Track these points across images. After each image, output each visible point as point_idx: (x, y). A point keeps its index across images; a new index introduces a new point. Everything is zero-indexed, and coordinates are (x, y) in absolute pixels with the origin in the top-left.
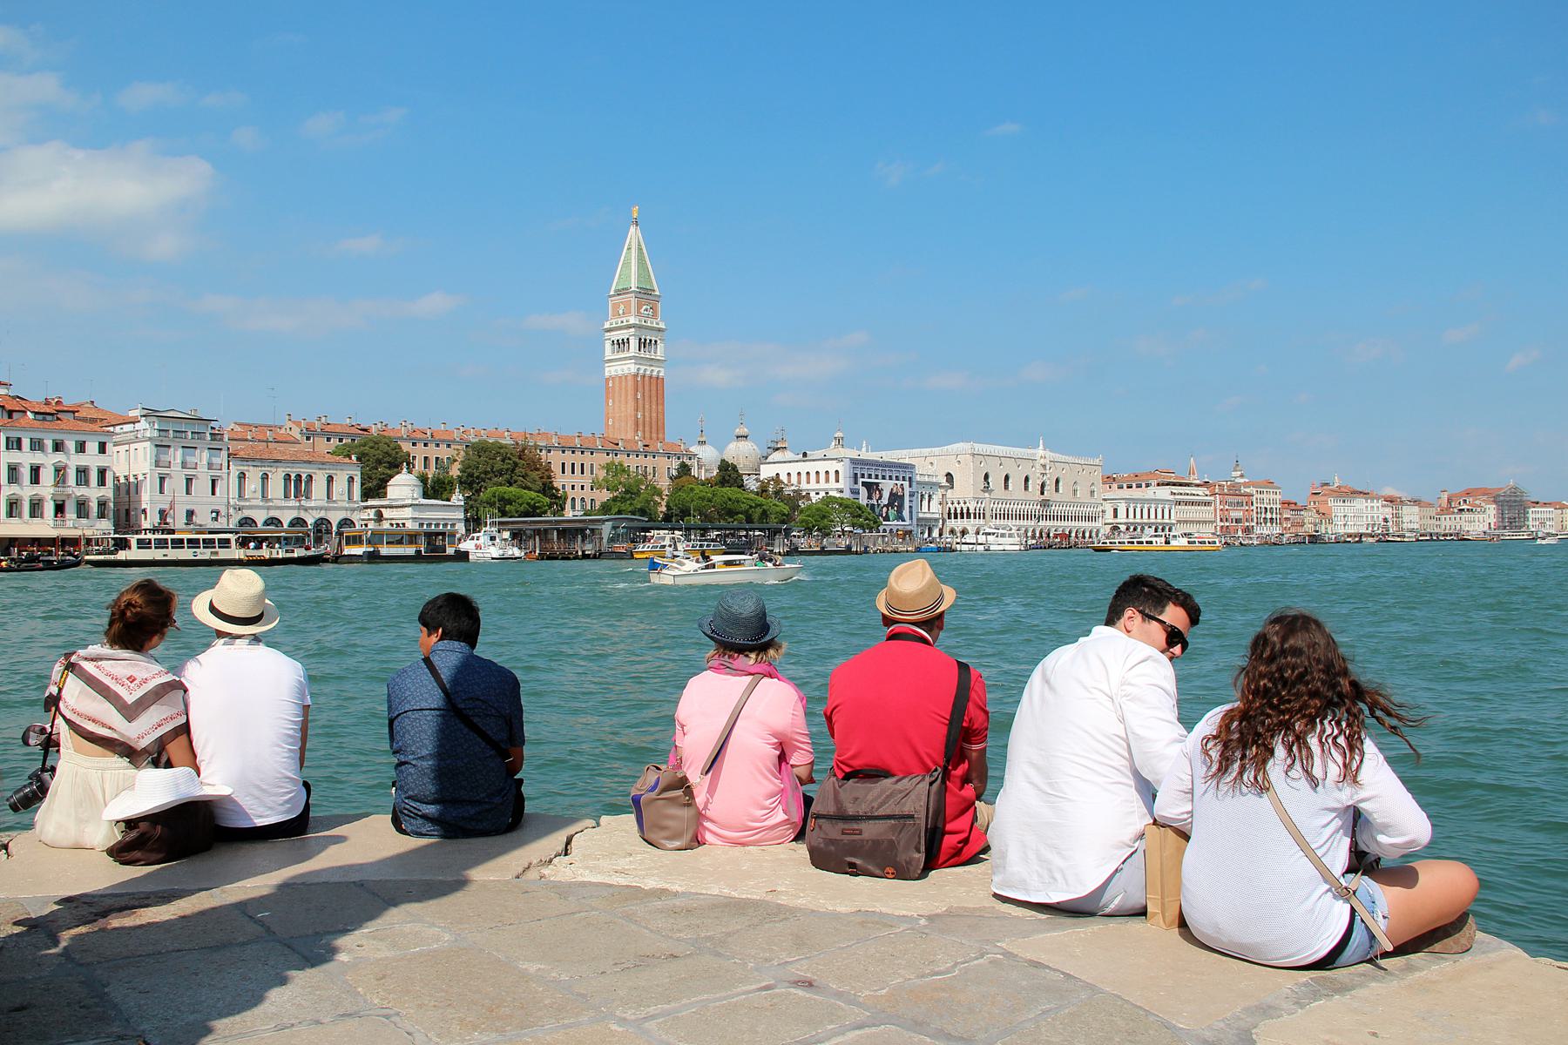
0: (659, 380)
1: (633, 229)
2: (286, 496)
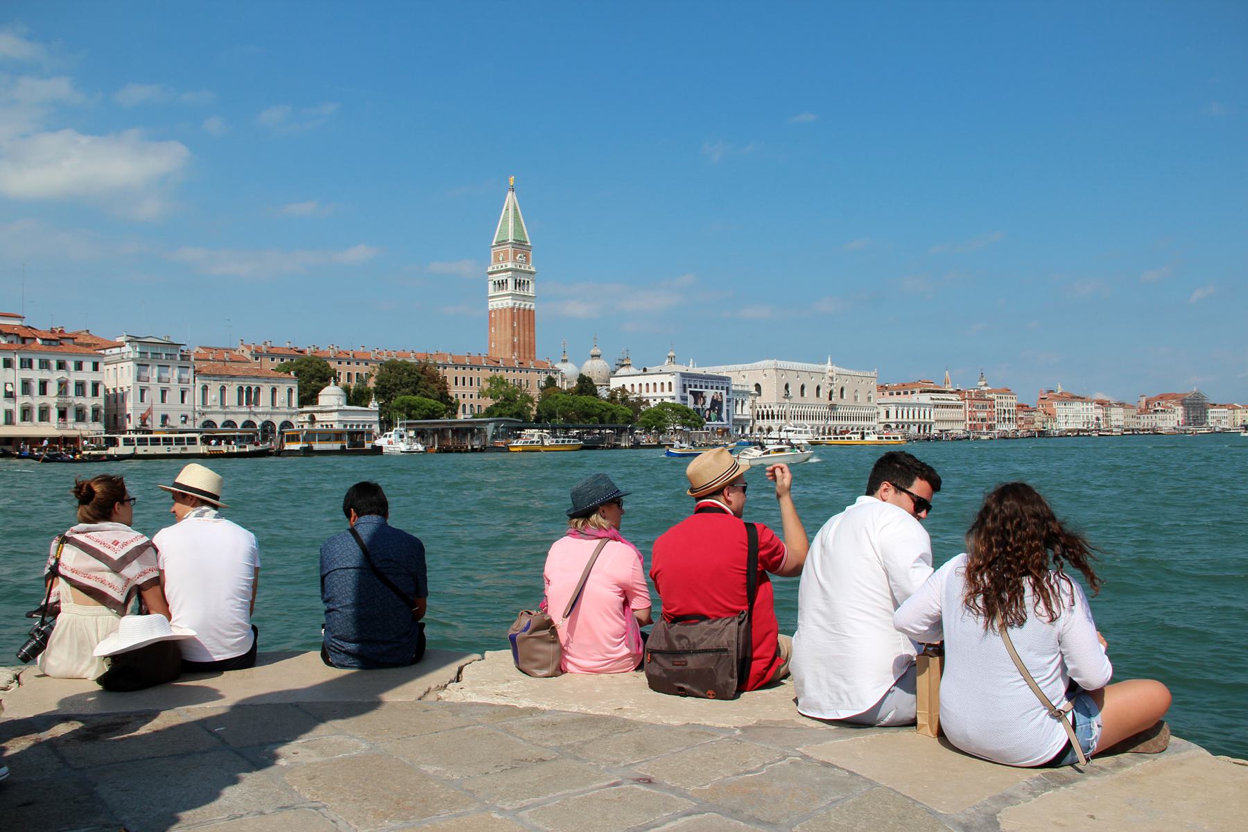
1: (510, 194)
2: (240, 404)
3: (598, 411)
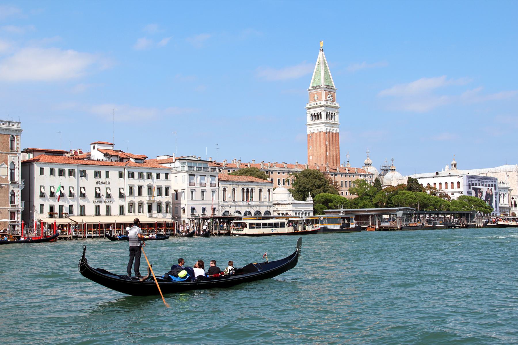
0: (336, 135)
1: (320, 53)
2: (243, 200)
3: (433, 202)
